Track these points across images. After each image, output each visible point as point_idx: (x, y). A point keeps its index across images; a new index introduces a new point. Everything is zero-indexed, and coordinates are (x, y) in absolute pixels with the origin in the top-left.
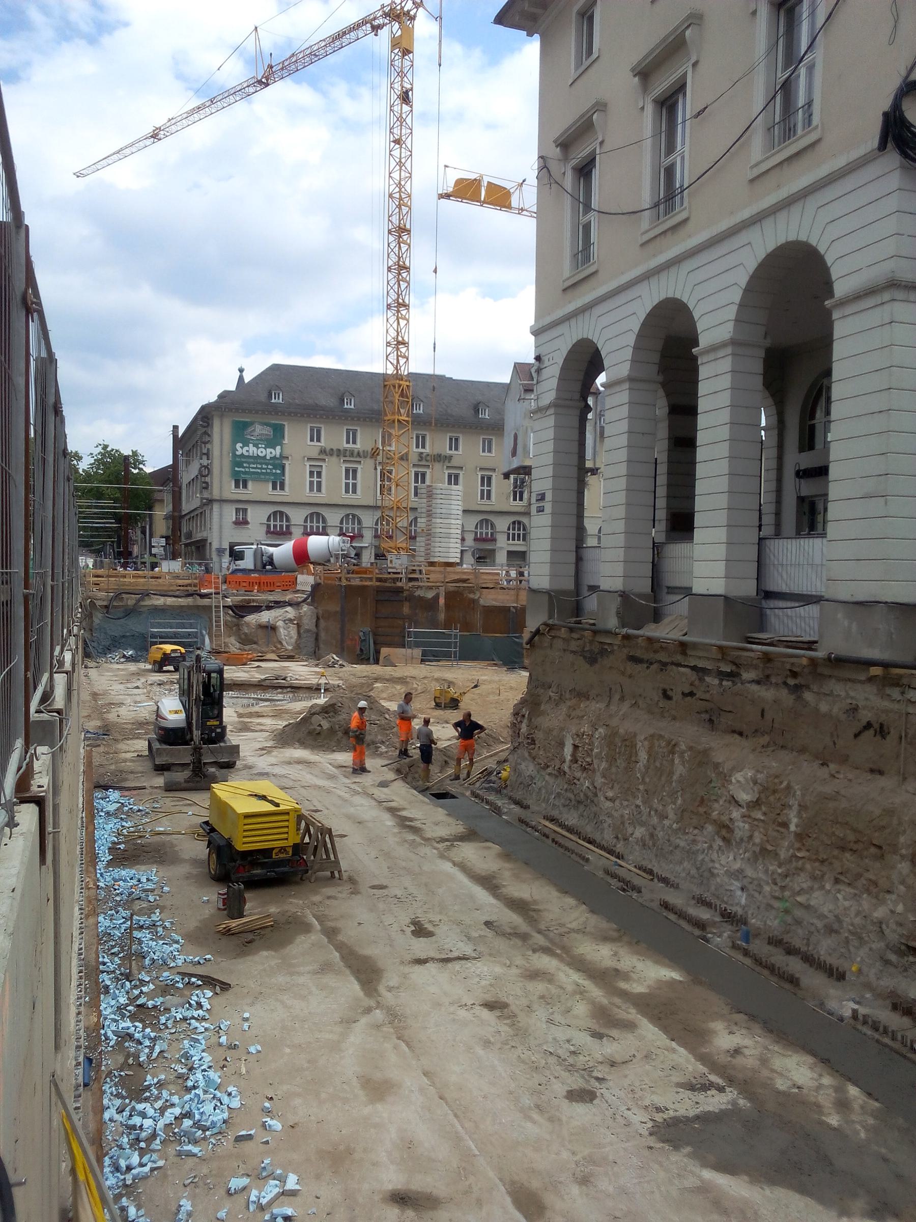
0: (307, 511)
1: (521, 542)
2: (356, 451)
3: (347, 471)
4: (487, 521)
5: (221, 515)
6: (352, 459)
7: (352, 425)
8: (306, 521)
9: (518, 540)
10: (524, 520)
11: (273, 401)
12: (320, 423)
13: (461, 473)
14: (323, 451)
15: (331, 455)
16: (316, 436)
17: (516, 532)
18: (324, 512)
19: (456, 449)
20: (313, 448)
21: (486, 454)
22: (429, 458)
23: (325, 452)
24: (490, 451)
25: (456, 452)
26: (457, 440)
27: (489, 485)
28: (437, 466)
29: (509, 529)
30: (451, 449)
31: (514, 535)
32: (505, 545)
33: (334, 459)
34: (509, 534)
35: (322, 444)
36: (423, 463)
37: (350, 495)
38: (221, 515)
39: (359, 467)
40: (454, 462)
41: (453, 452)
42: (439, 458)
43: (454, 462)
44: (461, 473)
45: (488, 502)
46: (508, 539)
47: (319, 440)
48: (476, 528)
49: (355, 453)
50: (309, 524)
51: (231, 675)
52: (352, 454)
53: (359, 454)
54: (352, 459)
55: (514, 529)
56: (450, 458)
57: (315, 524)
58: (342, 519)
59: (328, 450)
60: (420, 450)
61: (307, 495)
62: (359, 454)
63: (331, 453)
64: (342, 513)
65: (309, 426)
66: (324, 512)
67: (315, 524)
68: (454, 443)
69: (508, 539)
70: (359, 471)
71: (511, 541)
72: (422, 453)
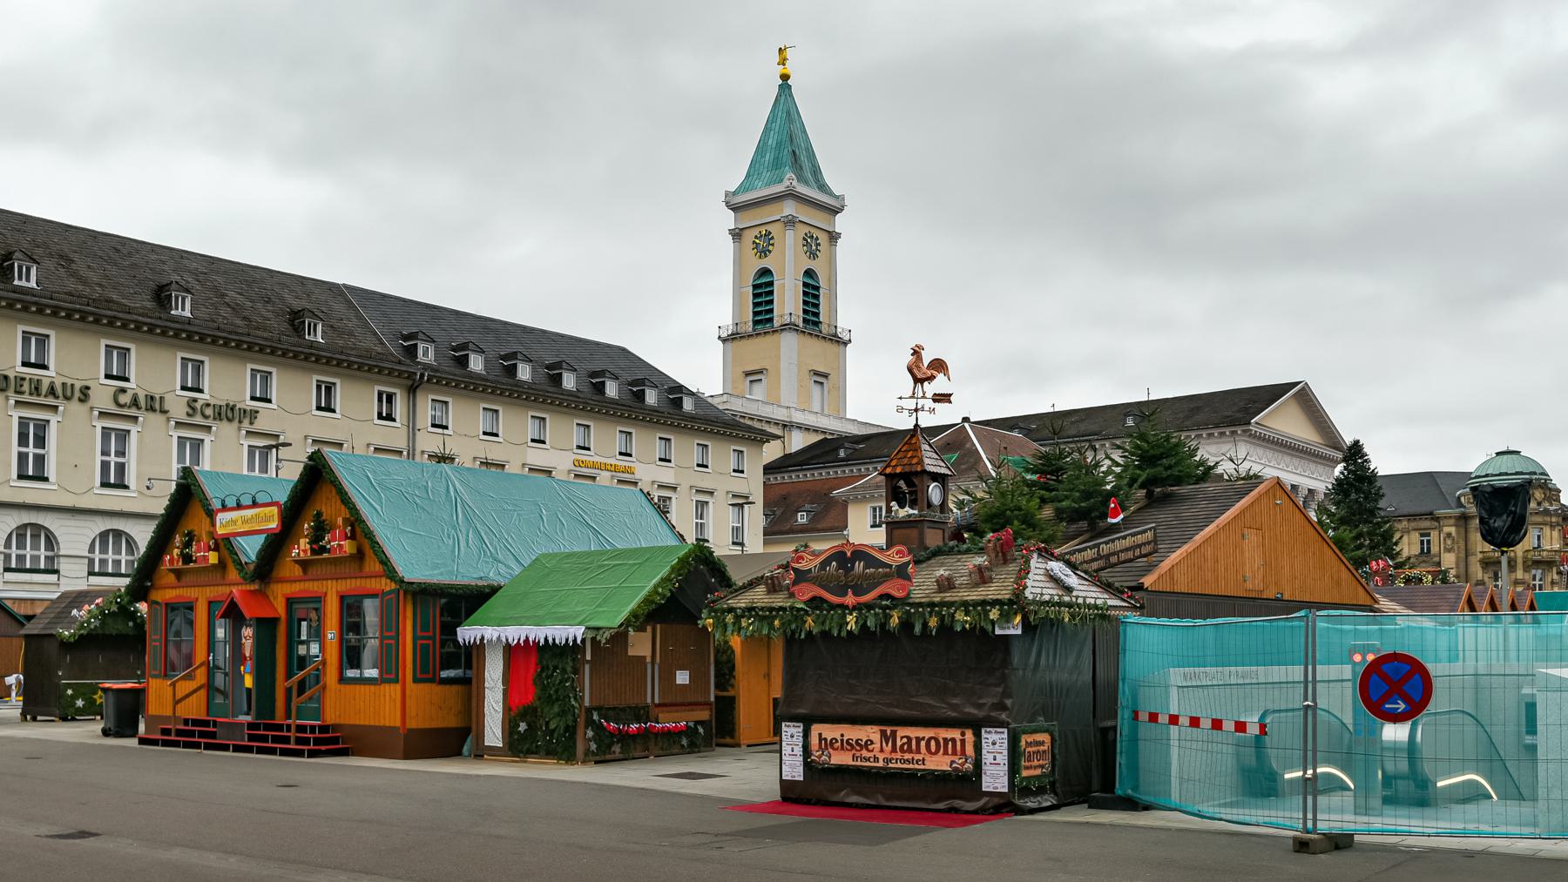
4: (118, 534)
6: (34, 399)
11: (16, 282)
12: (133, 340)
21: (69, 382)
22: (209, 412)
26: (328, 389)
27: (41, 441)
28: (225, 429)
36: (198, 420)
39: (54, 420)
42: (227, 413)
48: (91, 549)
50: (14, 551)
52: (36, 390)
53: (52, 391)
54: (34, 399)
56: (254, 414)
57: (28, 552)
58: (10, 535)
67: (110, 556)
72: (195, 400)
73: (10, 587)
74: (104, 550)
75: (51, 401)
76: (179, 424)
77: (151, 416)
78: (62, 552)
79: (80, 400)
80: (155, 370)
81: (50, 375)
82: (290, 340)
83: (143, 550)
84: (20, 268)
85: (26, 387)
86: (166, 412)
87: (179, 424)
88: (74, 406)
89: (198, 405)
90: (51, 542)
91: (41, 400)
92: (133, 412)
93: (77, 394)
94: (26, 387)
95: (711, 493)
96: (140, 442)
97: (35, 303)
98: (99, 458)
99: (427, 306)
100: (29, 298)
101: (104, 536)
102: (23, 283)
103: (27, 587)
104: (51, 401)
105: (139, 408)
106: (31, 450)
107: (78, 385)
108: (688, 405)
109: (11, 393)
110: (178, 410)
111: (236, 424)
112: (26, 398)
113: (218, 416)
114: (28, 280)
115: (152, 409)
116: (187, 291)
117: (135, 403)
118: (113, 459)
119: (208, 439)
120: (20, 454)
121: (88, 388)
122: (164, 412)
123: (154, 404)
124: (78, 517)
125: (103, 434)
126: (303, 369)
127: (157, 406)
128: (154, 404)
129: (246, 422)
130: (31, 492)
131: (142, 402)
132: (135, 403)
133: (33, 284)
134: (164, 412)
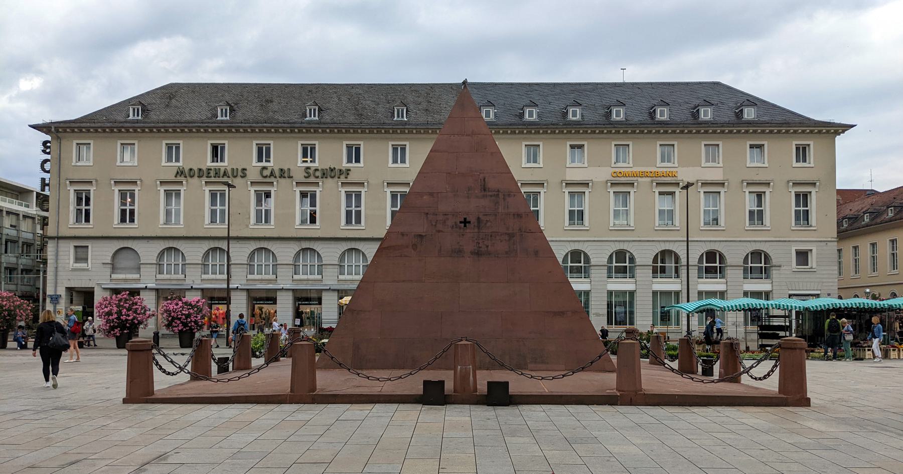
0: (206, 246)
7: (263, 138)
13: (768, 191)
14: (180, 172)
15: (192, 177)
16: (172, 151)
19: (403, 161)
20: (167, 168)
25: (357, 165)
26: (804, 149)
28: (330, 182)
30: (349, 161)
33: (195, 181)
35: (180, 164)
36: (312, 179)
40: (352, 178)
41: (354, 165)
42: (329, 173)
43: (352, 178)
44: (768, 191)
47: (177, 160)
51: (463, 419)
52: (217, 174)
53: (225, 174)
59: (187, 171)
60: (264, 164)
61: (342, 228)
62: (225, 174)
63: (191, 173)
64: (295, 247)
65: (345, 143)
66: (360, 246)
68: (355, 154)
70: (136, 193)
73: (251, 282)
77: (282, 181)
80: (287, 153)
81: (224, 164)
82: (695, 121)
83: (370, 260)
85: (212, 173)
89: (311, 171)
93: (240, 173)
94: (212, 173)
95: (135, 183)
96: (817, 199)
97: (250, 127)
98: (91, 207)
99: (669, 84)
100: (136, 125)
102: (224, 118)
103: (305, 282)
106: (128, 208)
108: (749, 114)
111: (336, 179)
112: (213, 179)
113: (324, 175)
114: (403, 117)
118: (353, 209)
121: (244, 169)
123: (284, 174)
124: (241, 242)
126: (382, 139)
128: (284, 174)
129: (342, 177)
130: (129, 229)
131: (277, 173)
132: (272, 174)
133: (317, 118)
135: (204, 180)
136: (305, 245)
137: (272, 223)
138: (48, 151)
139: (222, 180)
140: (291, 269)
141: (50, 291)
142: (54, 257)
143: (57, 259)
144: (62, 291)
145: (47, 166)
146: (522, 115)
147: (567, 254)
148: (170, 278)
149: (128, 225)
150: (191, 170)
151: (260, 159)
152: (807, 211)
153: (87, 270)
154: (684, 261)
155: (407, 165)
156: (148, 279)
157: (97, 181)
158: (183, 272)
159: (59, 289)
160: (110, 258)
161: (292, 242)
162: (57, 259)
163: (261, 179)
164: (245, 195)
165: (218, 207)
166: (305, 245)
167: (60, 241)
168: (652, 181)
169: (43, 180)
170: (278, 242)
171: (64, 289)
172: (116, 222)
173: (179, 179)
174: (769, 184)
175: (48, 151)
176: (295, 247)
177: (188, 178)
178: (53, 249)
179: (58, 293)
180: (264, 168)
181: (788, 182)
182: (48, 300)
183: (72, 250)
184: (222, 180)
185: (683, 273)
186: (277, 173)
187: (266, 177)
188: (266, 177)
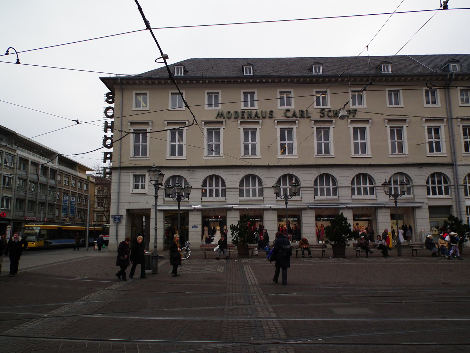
1: (444, 196)
2: (254, 112)
3: (355, 130)
4: (365, 175)
5: (120, 179)
8: (353, 183)
9: (441, 193)
10: (447, 172)
14: (220, 115)
15: (229, 118)
16: (213, 97)
17: (437, 185)
18: (296, 173)
23: (222, 115)
24: (397, 103)
25: (360, 106)
29: (428, 182)
31: (434, 188)
32: (426, 201)
33: (232, 122)
34: (428, 188)
35: (220, 107)
36: (326, 118)
37: (323, 155)
38: (120, 179)
39: (295, 127)
40: (359, 116)
45: (438, 154)
46: (429, 194)
49: (253, 115)
53: (257, 115)
55: (433, 182)
58: (316, 180)
59: (225, 114)
60: (321, 107)
62: (257, 115)
64: (315, 174)
65: (242, 91)
66: (296, 173)
69: (429, 194)
71: (431, 196)
74: (359, 183)
75: (256, 120)
76: (316, 122)
77: (302, 120)
78: (339, 185)
79: (269, 118)
84: (384, 67)
85: (246, 115)
86: (310, 117)
87: (316, 122)
88: (267, 121)
90: (334, 182)
91: (252, 120)
92: (294, 119)
93: (268, 115)
94: (246, 115)
95: (147, 124)
96: (298, 133)
101: (358, 176)
104: (256, 120)
105: (297, 117)
107: (268, 111)
109: (239, 119)
110: (317, 116)
112: (246, 120)
115: (302, 116)
116: (320, 64)
117: (294, 115)
118: (177, 143)
119: (295, 127)
120: (281, 144)
121: (272, 112)
122: (309, 117)
123: (303, 115)
125: (244, 132)
127: (305, 116)
128: (303, 115)
131: (260, 115)
132: (294, 115)
134: (309, 117)
135: (240, 120)
136: (323, 171)
137: (148, 155)
138: (110, 100)
139: (250, 120)
140: (312, 192)
141: (113, 212)
142: (117, 184)
143: (119, 186)
144: (123, 213)
145: (110, 112)
146: (311, 70)
147: (428, 178)
148: (326, 200)
149: (250, 156)
150: (229, 112)
151: (318, 104)
152: (439, 142)
153: (145, 194)
154: (452, 182)
155: (365, 106)
156: (270, 200)
157: (152, 122)
158: (335, 194)
159: (120, 210)
160: (238, 184)
161: (312, 169)
162: (119, 186)
163: (284, 119)
164: (267, 133)
165: (177, 143)
166: (323, 171)
167: (122, 171)
168: (384, 119)
169: (106, 123)
170: (301, 169)
171: (125, 210)
172: (168, 156)
173: (219, 120)
174: (368, 120)
175: (110, 100)
176: (315, 174)
177: (226, 119)
178: (117, 177)
179: (120, 214)
180: (288, 110)
181: (384, 119)
182: (111, 220)
183: (132, 178)
184: (250, 120)
185: (452, 190)
186: (298, 114)
187: (289, 117)
188: (289, 117)
